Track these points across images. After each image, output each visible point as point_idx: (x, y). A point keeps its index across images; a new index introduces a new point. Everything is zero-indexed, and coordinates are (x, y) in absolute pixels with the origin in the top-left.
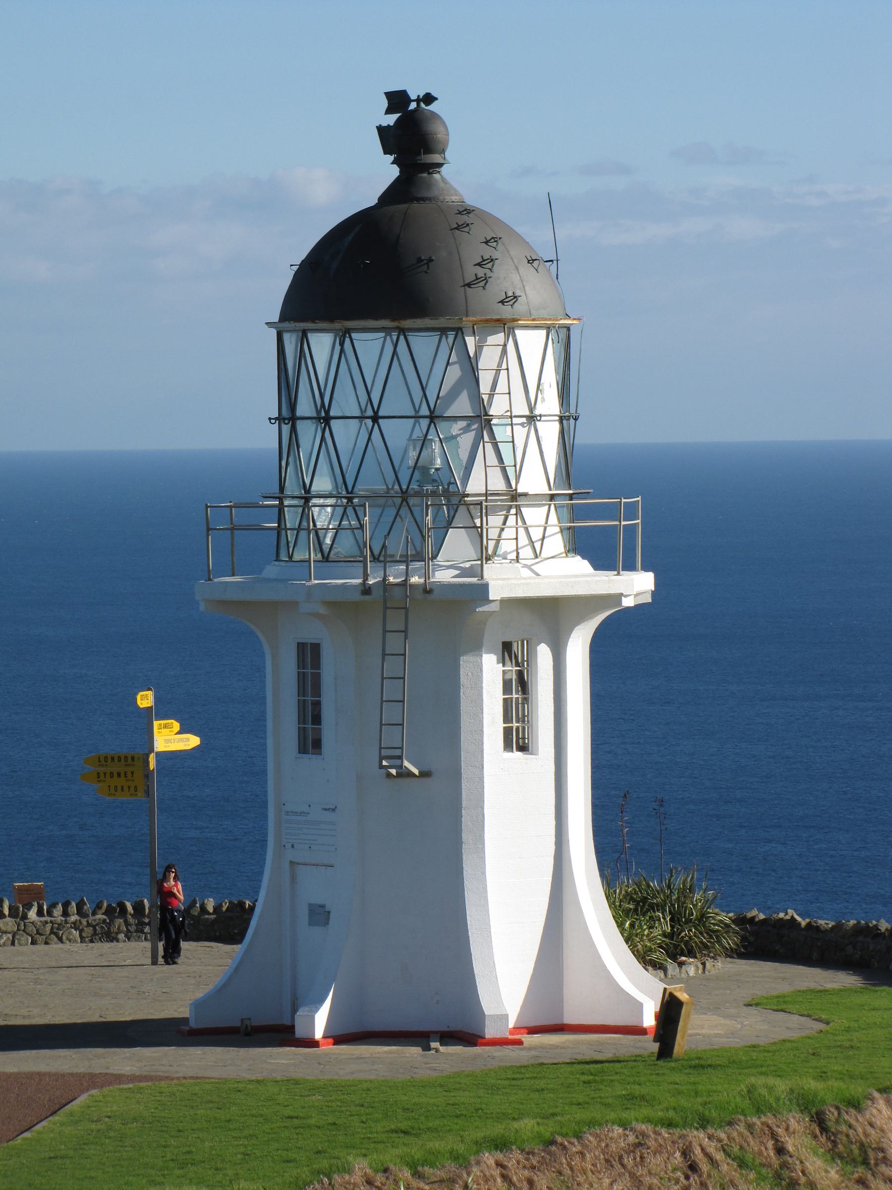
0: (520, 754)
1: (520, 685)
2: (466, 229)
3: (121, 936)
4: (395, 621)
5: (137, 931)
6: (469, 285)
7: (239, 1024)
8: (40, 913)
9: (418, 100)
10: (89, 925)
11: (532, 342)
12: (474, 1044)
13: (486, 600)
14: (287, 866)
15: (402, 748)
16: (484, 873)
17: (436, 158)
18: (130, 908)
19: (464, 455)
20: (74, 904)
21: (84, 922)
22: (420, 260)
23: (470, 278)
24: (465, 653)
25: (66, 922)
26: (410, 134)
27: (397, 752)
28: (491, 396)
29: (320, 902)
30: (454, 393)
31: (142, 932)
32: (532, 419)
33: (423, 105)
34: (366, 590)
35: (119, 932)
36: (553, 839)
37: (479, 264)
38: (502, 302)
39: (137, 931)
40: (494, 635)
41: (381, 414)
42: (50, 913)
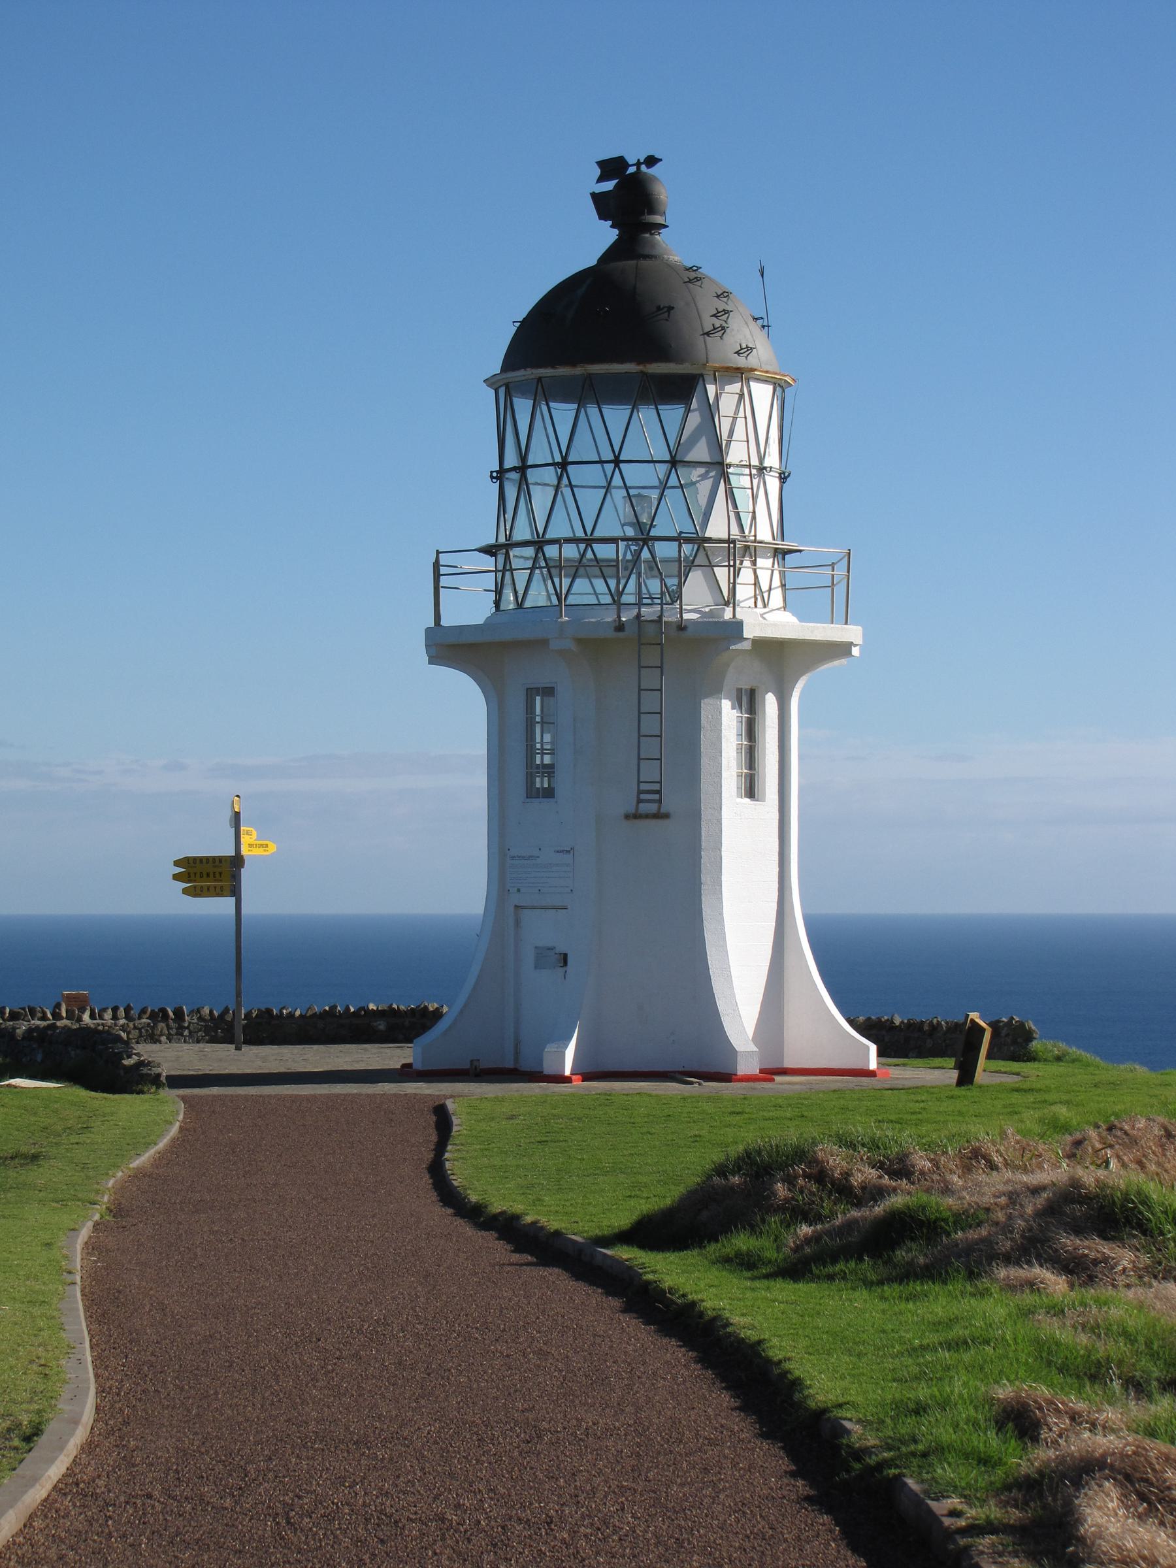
0: (748, 800)
1: (751, 731)
2: (699, 283)
3: (163, 1039)
4: (651, 656)
5: (177, 1034)
6: (708, 334)
7: (468, 1066)
8: (92, 1016)
9: (638, 164)
10: (135, 1028)
11: (762, 393)
12: (729, 1081)
13: (741, 638)
14: (512, 909)
15: (660, 782)
16: (721, 914)
17: (658, 219)
18: (171, 1014)
19: (703, 501)
20: (122, 1009)
21: (131, 1025)
22: (659, 308)
23: (708, 328)
24: (706, 696)
25: (116, 1025)
26: (628, 198)
27: (656, 787)
28: (729, 442)
29: (550, 945)
30: (694, 439)
31: (182, 1035)
32: (761, 469)
33: (643, 168)
34: (620, 627)
35: (162, 1035)
36: (776, 885)
37: (714, 315)
38: (738, 353)
39: (177, 1034)
40: (736, 678)
41: (622, 458)
42: (101, 1017)
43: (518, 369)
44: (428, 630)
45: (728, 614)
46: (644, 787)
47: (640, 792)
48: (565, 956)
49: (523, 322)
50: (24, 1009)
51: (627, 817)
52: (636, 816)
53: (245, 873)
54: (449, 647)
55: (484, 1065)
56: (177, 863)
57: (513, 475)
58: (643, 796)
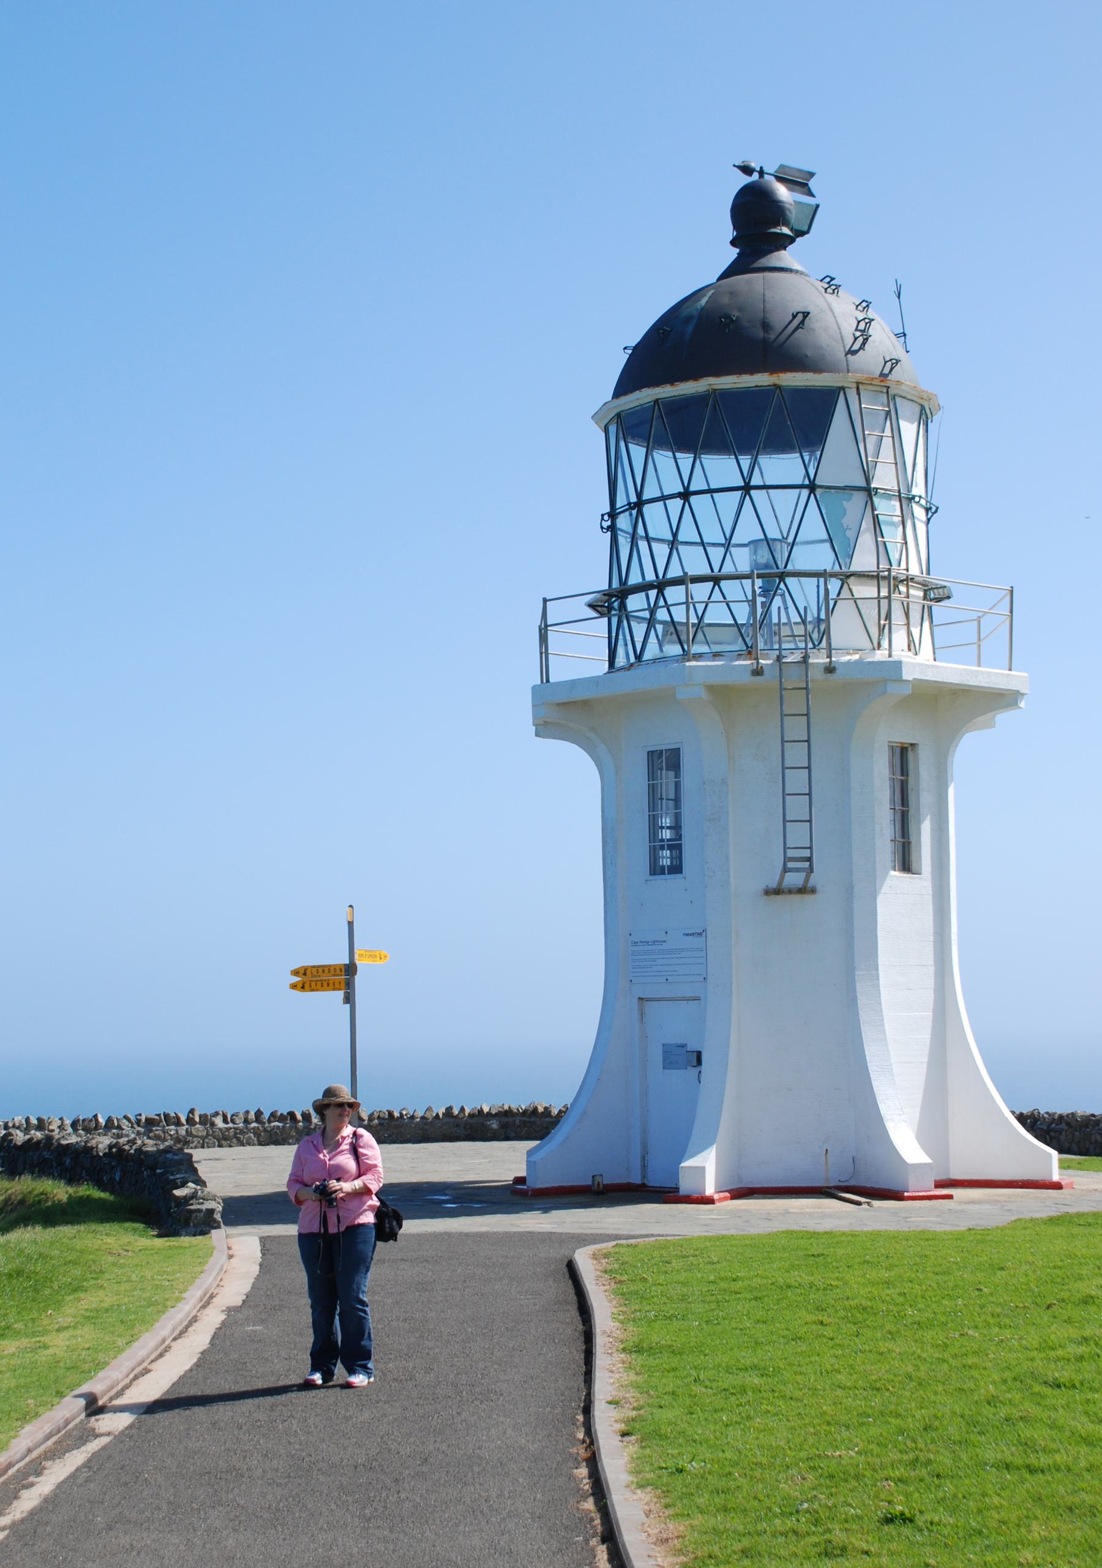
15: (811, 848)
29: (679, 1042)
43: (632, 391)
44: (534, 688)
45: (881, 655)
46: (791, 853)
47: (787, 859)
48: (699, 1055)
49: (635, 348)
50: (159, 1115)
51: (768, 892)
52: (778, 891)
53: (358, 979)
54: (563, 712)
55: (610, 1178)
56: (296, 973)
57: (624, 514)
58: (790, 865)
